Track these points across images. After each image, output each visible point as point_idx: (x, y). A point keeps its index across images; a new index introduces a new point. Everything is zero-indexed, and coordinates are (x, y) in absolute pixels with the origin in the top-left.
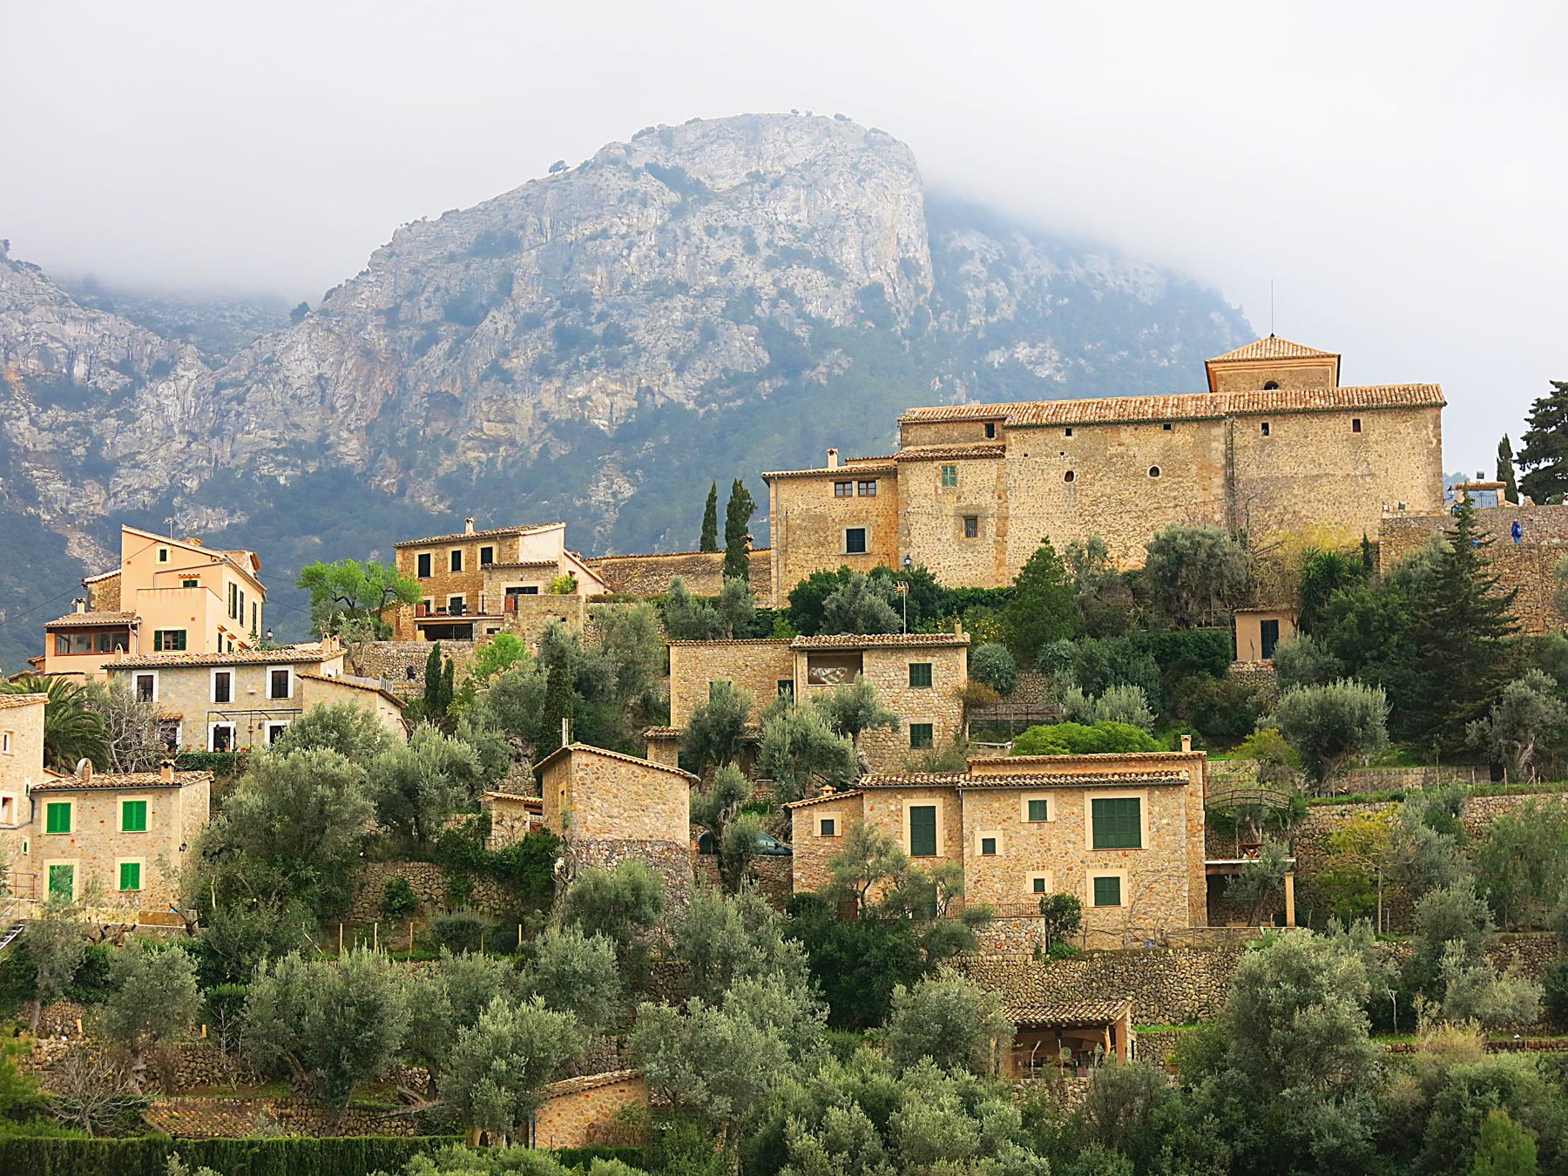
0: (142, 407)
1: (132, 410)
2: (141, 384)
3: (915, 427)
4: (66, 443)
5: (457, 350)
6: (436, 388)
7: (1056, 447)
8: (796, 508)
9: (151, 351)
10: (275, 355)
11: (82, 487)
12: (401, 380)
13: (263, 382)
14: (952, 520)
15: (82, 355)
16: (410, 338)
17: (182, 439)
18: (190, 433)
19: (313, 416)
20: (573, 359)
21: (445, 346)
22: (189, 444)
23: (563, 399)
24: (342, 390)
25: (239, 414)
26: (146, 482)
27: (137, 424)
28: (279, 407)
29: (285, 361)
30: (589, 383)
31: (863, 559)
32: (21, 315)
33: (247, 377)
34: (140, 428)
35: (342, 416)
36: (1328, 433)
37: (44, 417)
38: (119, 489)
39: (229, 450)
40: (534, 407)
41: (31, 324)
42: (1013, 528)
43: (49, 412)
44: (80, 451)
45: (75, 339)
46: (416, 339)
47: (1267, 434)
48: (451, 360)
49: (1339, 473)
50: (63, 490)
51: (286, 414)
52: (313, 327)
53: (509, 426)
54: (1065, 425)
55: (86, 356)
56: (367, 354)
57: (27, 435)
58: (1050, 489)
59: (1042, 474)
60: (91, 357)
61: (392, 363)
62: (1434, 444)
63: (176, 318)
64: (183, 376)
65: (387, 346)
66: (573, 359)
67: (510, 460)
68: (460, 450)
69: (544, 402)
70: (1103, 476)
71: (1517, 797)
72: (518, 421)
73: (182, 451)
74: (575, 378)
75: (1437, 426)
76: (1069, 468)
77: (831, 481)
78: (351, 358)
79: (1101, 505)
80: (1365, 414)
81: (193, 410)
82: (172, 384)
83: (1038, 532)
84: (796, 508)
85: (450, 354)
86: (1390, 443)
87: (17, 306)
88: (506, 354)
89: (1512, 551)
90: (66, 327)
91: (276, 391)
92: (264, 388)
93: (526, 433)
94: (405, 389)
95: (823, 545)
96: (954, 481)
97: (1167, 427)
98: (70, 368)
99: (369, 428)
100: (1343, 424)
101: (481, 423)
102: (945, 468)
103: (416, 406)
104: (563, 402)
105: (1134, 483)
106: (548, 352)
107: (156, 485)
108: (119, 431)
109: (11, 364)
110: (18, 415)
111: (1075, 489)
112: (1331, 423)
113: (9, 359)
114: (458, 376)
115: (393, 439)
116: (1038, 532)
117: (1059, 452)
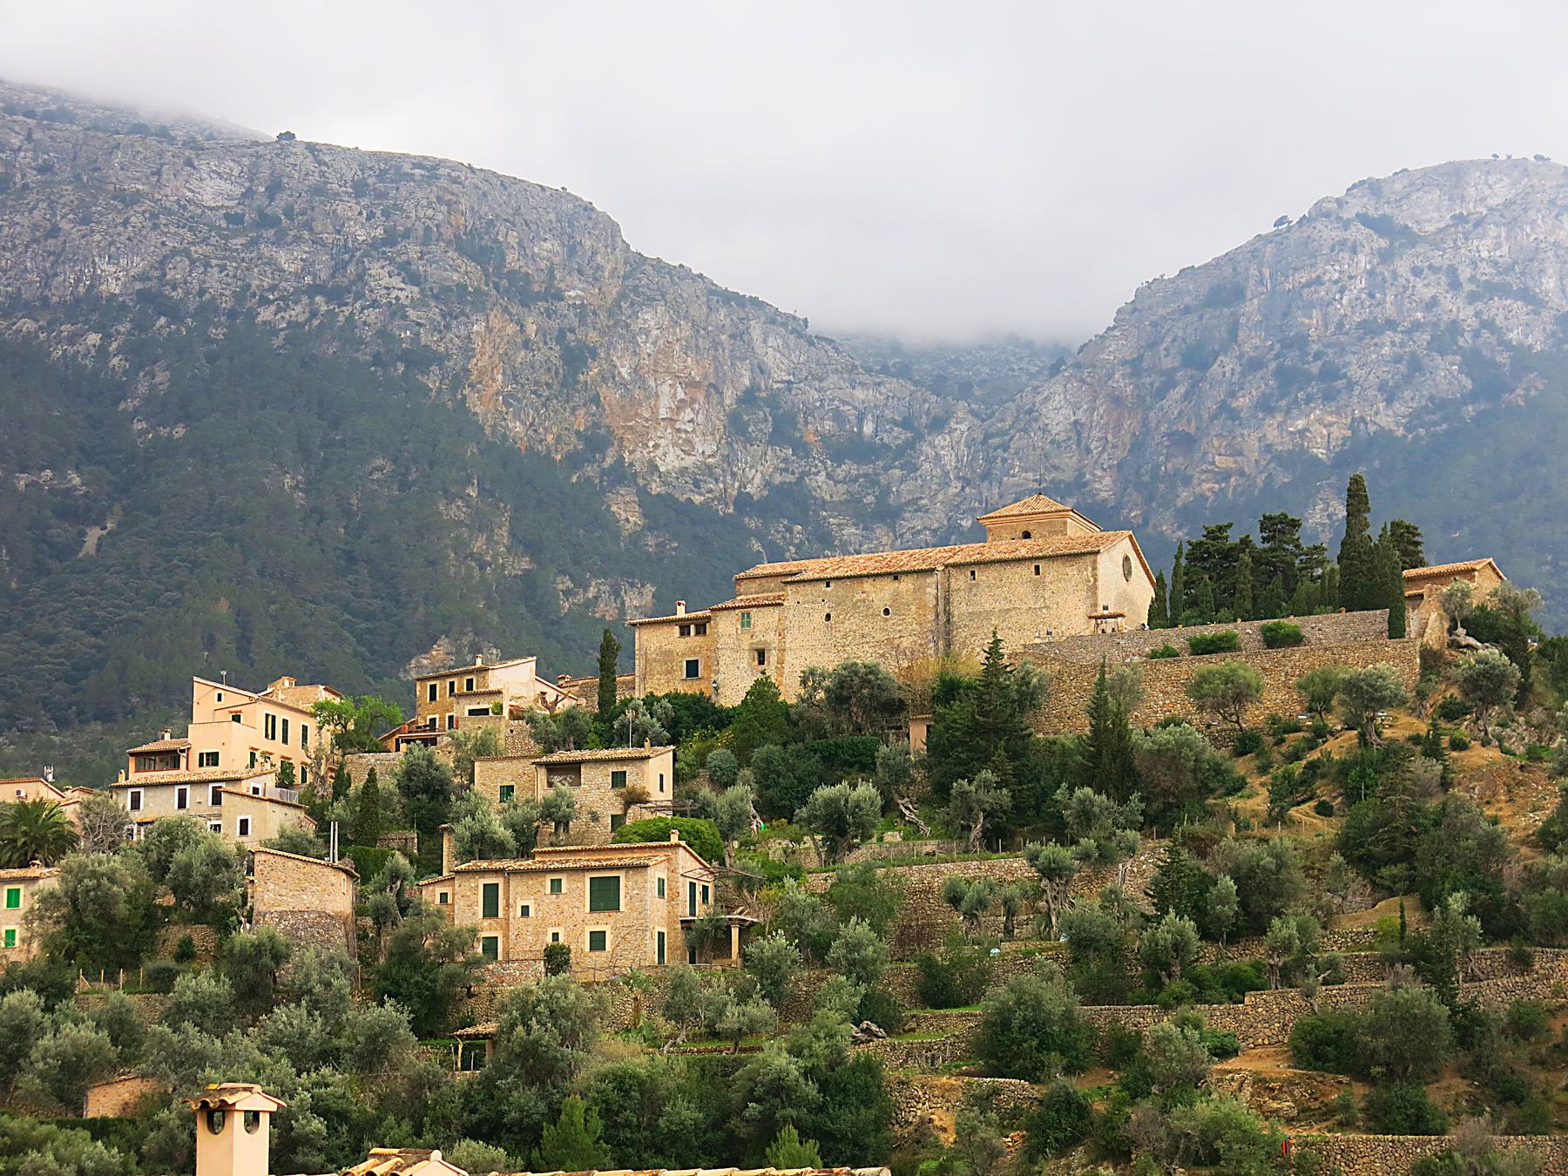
2: (920, 437)
4: (859, 493)
6: (1175, 428)
12: (1145, 422)
13: (1025, 431)
16: (1152, 384)
21: (1182, 389)
22: (963, 488)
25: (1004, 460)
32: (817, 384)
33: (1011, 427)
42: (789, 658)
49: (1024, 607)
52: (1068, 379)
53: (1238, 459)
56: (1116, 400)
57: (825, 487)
68: (1195, 482)
73: (957, 495)
74: (1295, 412)
75: (1094, 569)
76: (828, 611)
78: (1102, 404)
82: (947, 437)
85: (1186, 397)
88: (1233, 394)
90: (856, 392)
91: (1036, 437)
97: (896, 578)
99: (1120, 466)
100: (1027, 570)
107: (936, 525)
109: (810, 427)
115: (1138, 474)
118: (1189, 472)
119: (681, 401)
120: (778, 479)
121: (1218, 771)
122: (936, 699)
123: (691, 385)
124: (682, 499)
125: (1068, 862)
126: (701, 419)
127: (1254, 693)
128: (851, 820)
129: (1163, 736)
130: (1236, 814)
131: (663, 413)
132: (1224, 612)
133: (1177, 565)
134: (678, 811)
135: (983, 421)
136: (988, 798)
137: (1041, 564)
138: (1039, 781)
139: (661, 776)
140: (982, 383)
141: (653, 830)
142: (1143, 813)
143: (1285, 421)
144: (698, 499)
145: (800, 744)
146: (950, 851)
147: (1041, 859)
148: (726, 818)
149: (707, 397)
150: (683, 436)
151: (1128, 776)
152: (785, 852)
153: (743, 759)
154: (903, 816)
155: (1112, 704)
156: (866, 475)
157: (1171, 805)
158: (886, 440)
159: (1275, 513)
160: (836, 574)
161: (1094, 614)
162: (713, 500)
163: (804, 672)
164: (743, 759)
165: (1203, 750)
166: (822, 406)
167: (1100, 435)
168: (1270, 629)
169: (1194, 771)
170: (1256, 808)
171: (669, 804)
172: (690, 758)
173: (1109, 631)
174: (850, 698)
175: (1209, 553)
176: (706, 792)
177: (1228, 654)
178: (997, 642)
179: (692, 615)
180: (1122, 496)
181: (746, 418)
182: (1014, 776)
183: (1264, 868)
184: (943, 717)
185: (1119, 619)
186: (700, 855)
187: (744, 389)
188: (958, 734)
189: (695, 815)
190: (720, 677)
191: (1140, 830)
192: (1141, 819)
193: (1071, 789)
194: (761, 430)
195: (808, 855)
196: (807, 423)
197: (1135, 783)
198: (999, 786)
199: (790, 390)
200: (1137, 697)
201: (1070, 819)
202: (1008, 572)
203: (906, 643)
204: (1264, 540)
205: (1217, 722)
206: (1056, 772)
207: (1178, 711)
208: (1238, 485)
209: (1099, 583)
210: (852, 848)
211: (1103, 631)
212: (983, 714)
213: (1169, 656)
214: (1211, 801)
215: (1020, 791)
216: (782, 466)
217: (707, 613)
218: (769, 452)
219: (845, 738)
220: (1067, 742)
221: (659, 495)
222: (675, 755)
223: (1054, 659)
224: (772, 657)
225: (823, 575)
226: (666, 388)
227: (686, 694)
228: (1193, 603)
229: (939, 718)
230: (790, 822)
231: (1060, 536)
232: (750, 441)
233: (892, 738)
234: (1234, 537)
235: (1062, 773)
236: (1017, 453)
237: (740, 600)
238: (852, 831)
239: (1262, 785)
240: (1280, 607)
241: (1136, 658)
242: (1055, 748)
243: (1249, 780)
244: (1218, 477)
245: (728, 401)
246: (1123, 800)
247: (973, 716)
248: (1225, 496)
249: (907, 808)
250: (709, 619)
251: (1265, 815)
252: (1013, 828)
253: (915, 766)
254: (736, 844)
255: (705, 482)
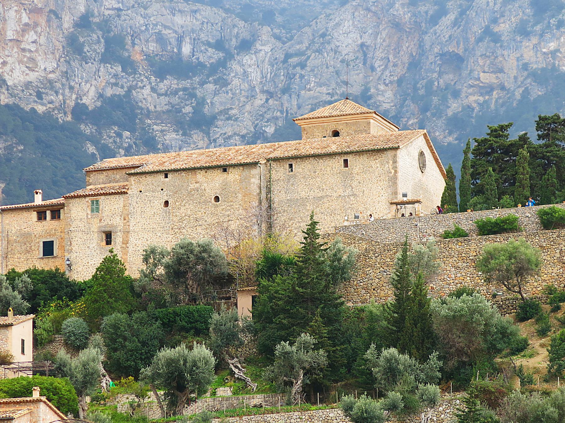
0: (232, 75)
1: (225, 77)
2: (229, 56)
3: (94, 173)
4: (178, 104)
5: (460, 20)
6: (446, 49)
7: (158, 186)
8: (13, 229)
9: (237, 32)
10: (327, 30)
11: (190, 136)
12: (421, 46)
13: (319, 51)
14: (96, 235)
15: (188, 38)
16: (426, 12)
17: (262, 97)
18: (268, 92)
19: (358, 74)
20: (546, 22)
21: (451, 17)
22: (267, 100)
23: (539, 53)
24: (379, 54)
25: (302, 77)
26: (237, 130)
27: (229, 87)
28: (331, 69)
29: (336, 34)
30: (558, 39)
31: (53, 260)
32: (142, 11)
33: (307, 48)
34: (231, 90)
35: (380, 73)
36: (328, 169)
37: (161, 85)
38: (217, 136)
39: (296, 103)
40: (518, 60)
41: (150, 17)
42: (132, 239)
43: (165, 81)
44: (188, 109)
45: (182, 27)
46: (431, 12)
47: (292, 171)
48: (456, 28)
49: (335, 195)
50: (176, 139)
51: (337, 74)
52: (356, 8)
53: (500, 75)
54: (164, 171)
55: (190, 39)
56: (397, 26)
57: (149, 99)
58: (154, 213)
59: (150, 203)
60: (194, 39)
61: (415, 31)
62: (393, 173)
63: (273, 3)
64: (261, 50)
65: (410, 19)
66: (546, 22)
67: (501, 101)
68: (463, 95)
69: (525, 56)
70: (186, 203)
71: (268, 415)
72: (505, 71)
73: (262, 106)
74: (548, 36)
75: (395, 162)
76: (166, 198)
77: (34, 211)
78: (384, 29)
79: (185, 222)
80: (351, 155)
81: (269, 74)
82: (254, 56)
83: (147, 240)
84: (13, 229)
85: (455, 23)
86: (365, 173)
87: (139, 4)
88: (495, 21)
89: (392, 247)
90: (175, 18)
91: (328, 57)
92: (320, 56)
93: (512, 80)
94: (423, 50)
95: (29, 252)
96: (98, 210)
97: (225, 170)
98: (180, 48)
99: (400, 82)
100: (338, 162)
101: (479, 74)
102: (92, 202)
103: (432, 63)
104: (539, 55)
105: (204, 207)
106: (527, 17)
107: (244, 132)
108: (216, 93)
109: (136, 47)
110: (142, 85)
111: (169, 212)
112: (330, 162)
113: (135, 44)
114: (461, 39)
115: (415, 89)
116: (147, 240)
117: (160, 188)
118: (458, 87)
119: (26, 25)
120: (109, 92)
121: (504, 333)
122: (260, 273)
123: (35, 11)
124: (27, 108)
125: (378, 412)
126: (43, 40)
127: (534, 267)
128: (188, 377)
129: (457, 304)
130: (521, 371)
131: (10, 35)
132: (506, 198)
133: (466, 159)
134: (37, 370)
135: (284, 43)
136: (307, 357)
137: (350, 158)
138: (350, 343)
139: (23, 341)
140: (283, 12)
141: (17, 387)
142: (441, 370)
143: (539, 43)
144: (40, 109)
145: (144, 313)
146: (274, 404)
147: (355, 410)
148: (80, 376)
149: (48, 21)
150: (28, 54)
151: (428, 338)
152: (131, 405)
153: (94, 327)
154: (232, 373)
155: (413, 279)
156: (185, 89)
157: (464, 363)
158: (201, 59)
159: (549, 114)
160: (173, 167)
161: (395, 201)
162: (54, 110)
163: (146, 251)
164: (94, 327)
165: (492, 316)
166: (147, 29)
167: (383, 55)
168: (546, 213)
169: (485, 333)
170: (537, 365)
171: (30, 365)
172: (48, 325)
173: (407, 215)
174: (186, 272)
175: (492, 149)
176: (62, 354)
177: (511, 234)
178: (314, 224)
179: (48, 202)
180: (402, 106)
181: (82, 40)
182: (329, 338)
183: (549, 417)
184: (266, 289)
185: (416, 205)
186: (58, 408)
187: (79, 15)
188: (280, 303)
189: (53, 374)
190: (73, 256)
191: (439, 384)
192: (439, 375)
193: (379, 349)
194: (95, 50)
195: (151, 408)
196: (134, 44)
197: (434, 344)
198: (316, 347)
199: (119, 16)
200: (432, 270)
201: (379, 376)
202: (322, 164)
203: (233, 226)
204: (540, 137)
205: (502, 292)
206: (365, 335)
207: (468, 283)
208: (500, 98)
209: (399, 174)
210: (189, 401)
211: (403, 215)
212: (301, 285)
213: (460, 236)
214: (498, 360)
215: (334, 352)
216: (113, 81)
217: (61, 200)
218: (102, 69)
219: (183, 307)
220: (374, 310)
221: (7, 106)
222: (34, 323)
223: (361, 239)
224: (118, 239)
225: (161, 168)
226: (12, 14)
227: (43, 270)
228: (479, 191)
229: (264, 290)
230: (136, 379)
231: (364, 135)
232: (85, 59)
233: (223, 307)
234: (513, 136)
235: (370, 335)
236: (313, 70)
237: (88, 190)
238: (190, 386)
239: (542, 346)
240: (554, 194)
241: (431, 238)
242: (363, 315)
243: (530, 342)
244: (483, 91)
245: (66, 25)
246: (424, 359)
247: (294, 288)
248: (488, 107)
249: (236, 367)
250: (62, 206)
251: (545, 371)
252: (328, 383)
253: (243, 331)
254: (88, 399)
255: (47, 94)
